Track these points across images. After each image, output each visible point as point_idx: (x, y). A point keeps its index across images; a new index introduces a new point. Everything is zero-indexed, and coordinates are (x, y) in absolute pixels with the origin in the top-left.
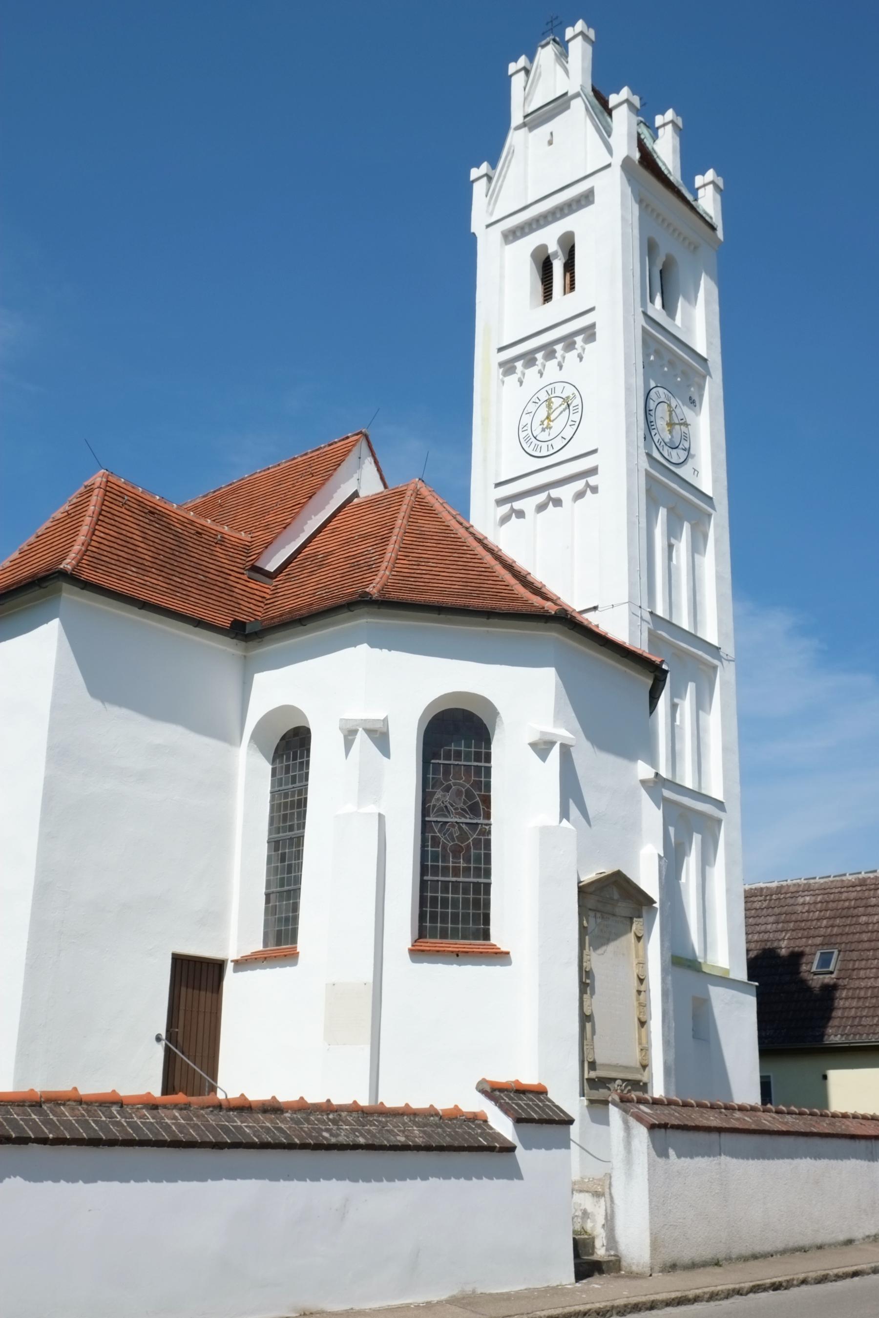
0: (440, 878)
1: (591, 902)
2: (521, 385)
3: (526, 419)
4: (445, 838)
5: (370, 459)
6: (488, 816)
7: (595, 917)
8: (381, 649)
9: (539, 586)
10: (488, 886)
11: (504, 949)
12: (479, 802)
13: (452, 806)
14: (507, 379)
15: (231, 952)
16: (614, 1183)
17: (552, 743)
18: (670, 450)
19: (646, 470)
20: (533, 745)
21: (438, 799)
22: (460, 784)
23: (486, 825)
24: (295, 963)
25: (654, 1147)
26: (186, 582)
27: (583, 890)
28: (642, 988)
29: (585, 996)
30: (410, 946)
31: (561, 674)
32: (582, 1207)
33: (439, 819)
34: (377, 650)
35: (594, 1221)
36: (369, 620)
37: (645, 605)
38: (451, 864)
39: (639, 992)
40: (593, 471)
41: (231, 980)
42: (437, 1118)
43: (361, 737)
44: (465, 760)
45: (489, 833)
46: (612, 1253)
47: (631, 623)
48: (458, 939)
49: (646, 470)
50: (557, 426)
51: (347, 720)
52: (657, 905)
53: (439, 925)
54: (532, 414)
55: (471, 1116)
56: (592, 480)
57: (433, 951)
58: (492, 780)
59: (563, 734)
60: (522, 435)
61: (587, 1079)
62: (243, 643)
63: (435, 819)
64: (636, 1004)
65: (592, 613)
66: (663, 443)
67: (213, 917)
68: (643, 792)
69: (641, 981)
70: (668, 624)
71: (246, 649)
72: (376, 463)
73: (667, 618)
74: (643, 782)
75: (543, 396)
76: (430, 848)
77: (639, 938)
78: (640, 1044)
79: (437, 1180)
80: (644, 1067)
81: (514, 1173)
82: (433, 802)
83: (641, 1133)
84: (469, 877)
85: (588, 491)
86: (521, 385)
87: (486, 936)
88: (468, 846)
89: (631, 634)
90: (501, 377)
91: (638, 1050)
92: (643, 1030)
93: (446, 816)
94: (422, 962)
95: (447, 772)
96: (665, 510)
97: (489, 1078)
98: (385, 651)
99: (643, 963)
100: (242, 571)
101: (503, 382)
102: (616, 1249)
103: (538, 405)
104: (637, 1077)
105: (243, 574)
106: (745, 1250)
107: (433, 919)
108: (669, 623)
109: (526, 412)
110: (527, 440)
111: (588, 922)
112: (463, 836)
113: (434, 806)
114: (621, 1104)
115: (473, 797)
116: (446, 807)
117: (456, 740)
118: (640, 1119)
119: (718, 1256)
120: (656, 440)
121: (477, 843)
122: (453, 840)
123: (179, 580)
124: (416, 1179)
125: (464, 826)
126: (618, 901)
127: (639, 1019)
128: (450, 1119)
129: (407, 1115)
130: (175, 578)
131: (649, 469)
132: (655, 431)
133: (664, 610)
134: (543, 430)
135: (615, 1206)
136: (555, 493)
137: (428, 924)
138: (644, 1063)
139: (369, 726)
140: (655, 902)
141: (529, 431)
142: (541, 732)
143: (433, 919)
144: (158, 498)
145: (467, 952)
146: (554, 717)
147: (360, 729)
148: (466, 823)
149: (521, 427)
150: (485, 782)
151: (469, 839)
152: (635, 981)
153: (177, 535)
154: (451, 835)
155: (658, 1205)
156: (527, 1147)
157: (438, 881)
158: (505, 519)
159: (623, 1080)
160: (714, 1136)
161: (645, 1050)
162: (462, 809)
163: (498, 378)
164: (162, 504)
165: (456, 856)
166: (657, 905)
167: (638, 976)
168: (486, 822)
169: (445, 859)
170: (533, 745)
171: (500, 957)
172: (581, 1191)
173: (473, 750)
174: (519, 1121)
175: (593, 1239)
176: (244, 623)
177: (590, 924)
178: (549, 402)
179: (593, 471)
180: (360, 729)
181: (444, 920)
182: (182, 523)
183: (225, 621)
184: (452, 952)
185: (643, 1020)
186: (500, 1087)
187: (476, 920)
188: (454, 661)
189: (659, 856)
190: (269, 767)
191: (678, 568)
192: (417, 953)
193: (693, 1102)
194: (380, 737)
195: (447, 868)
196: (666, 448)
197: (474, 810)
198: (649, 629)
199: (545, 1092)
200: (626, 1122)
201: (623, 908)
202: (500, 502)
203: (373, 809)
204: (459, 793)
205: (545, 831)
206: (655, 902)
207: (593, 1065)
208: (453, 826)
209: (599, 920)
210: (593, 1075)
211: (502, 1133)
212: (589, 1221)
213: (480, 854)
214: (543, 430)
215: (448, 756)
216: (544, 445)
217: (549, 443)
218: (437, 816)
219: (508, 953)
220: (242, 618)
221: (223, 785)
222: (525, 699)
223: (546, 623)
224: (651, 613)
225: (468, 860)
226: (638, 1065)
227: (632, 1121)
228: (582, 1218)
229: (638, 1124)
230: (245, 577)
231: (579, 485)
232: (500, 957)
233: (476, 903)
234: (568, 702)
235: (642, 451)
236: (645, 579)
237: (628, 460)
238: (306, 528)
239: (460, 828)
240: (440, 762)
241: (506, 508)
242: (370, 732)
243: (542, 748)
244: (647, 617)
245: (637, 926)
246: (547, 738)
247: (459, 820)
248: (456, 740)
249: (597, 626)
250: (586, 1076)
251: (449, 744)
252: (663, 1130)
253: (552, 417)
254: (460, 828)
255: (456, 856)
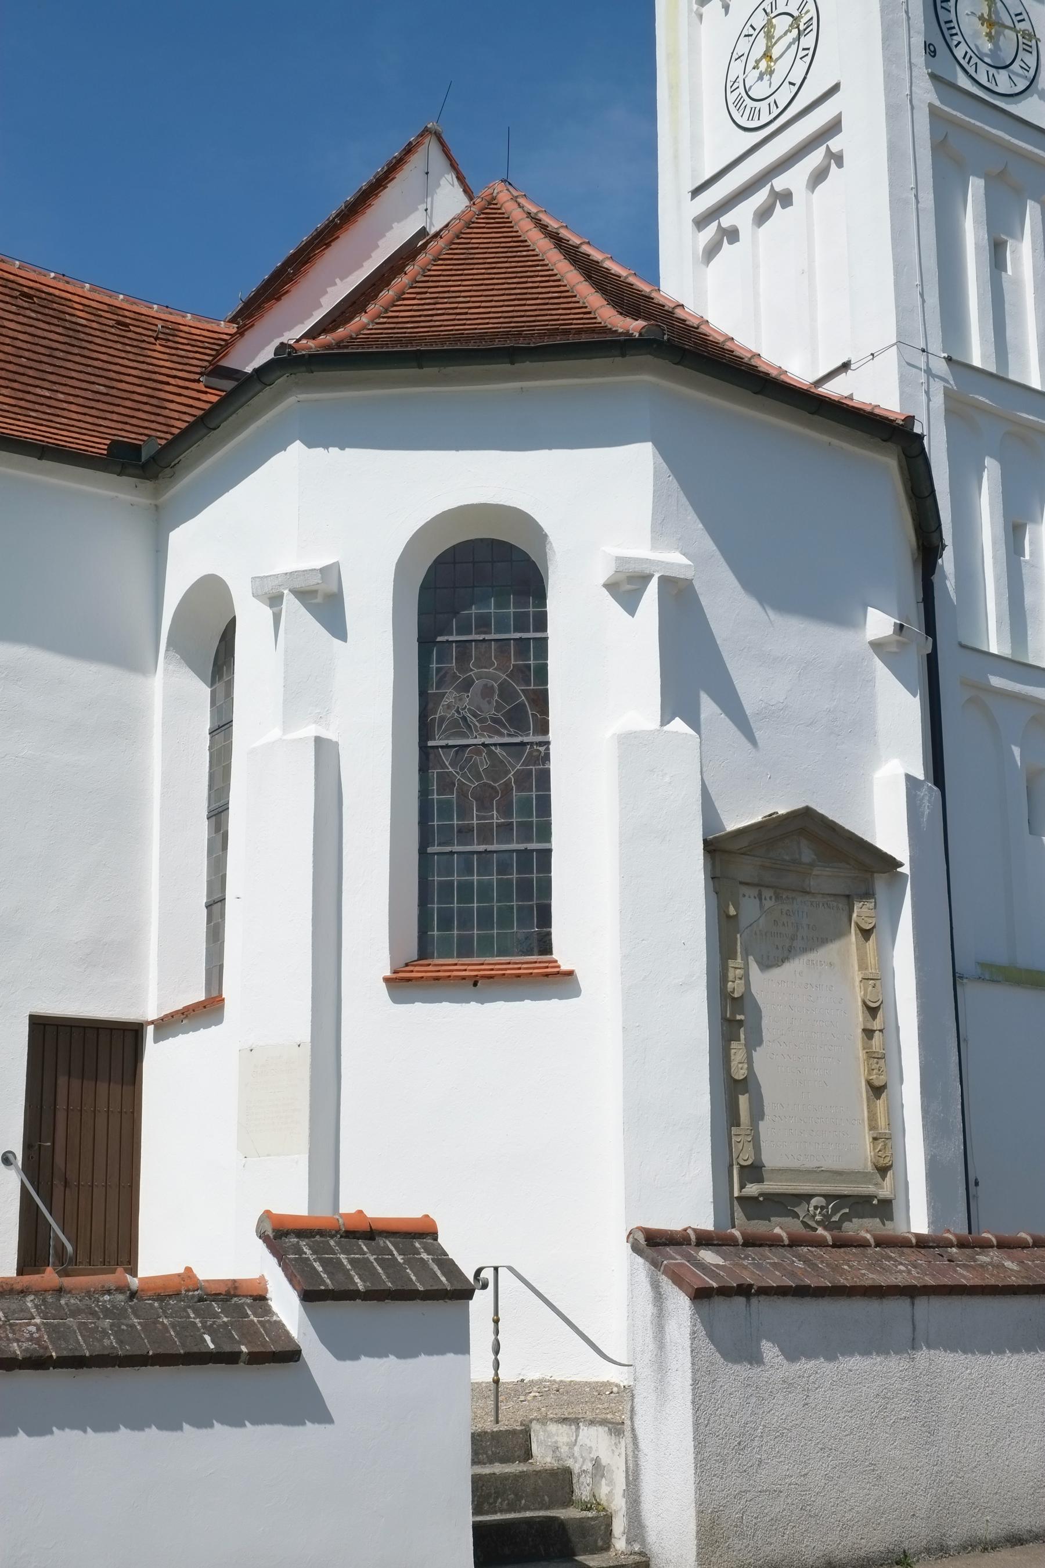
0: (457, 848)
1: (746, 868)
2: (727, 13)
3: (737, 67)
4: (464, 776)
5: (451, 177)
6: (543, 727)
7: (760, 897)
8: (326, 447)
9: (694, 322)
10: (546, 856)
11: (565, 967)
12: (527, 704)
13: (475, 715)
14: (704, 10)
15: (149, 1009)
16: (638, 1408)
17: (646, 578)
18: (992, 71)
19: (931, 105)
20: (611, 587)
21: (449, 707)
22: (488, 676)
23: (540, 744)
24: (219, 1020)
25: (711, 1336)
26: (61, 396)
27: (720, 851)
28: (877, 1025)
29: (734, 1045)
30: (388, 973)
31: (664, 450)
32: (593, 1455)
33: (451, 742)
34: (320, 451)
35: (611, 1483)
36: (302, 397)
37: (936, 346)
38: (475, 822)
39: (869, 1033)
40: (834, 127)
41: (159, 1059)
42: (120, 1297)
43: (290, 604)
44: (498, 631)
45: (547, 757)
46: (637, 1548)
47: (903, 380)
48: (493, 956)
49: (931, 105)
50: (781, 68)
51: (261, 578)
52: (905, 869)
53: (455, 932)
54: (744, 58)
55: (223, 1290)
56: (835, 144)
57: (428, 978)
58: (549, 662)
59: (674, 559)
60: (731, 98)
61: (739, 1198)
62: (149, 484)
63: (443, 743)
64: (862, 1054)
65: (842, 377)
66: (975, 60)
67: (115, 950)
68: (878, 664)
69: (872, 1011)
70: (998, 380)
71: (156, 494)
72: (461, 178)
73: (993, 369)
74: (877, 646)
75: (759, 20)
76: (435, 796)
77: (866, 934)
78: (873, 1127)
79: (77, 1434)
80: (883, 1170)
81: (311, 1408)
82: (440, 712)
83: (680, 1304)
84: (510, 841)
85: (833, 166)
86: (727, 13)
87: (545, 947)
88: (507, 784)
89: (904, 397)
90: (695, 7)
91: (868, 1140)
92: (880, 1104)
93: (464, 735)
94: (439, 1001)
95: (463, 657)
96: (1038, 207)
97: (275, 1211)
98: (334, 451)
99: (878, 979)
100: (197, 377)
101: (701, 16)
102: (643, 1542)
103: (752, 39)
104: (868, 1189)
105: (198, 381)
106: (991, 1527)
107: (446, 923)
108: (1000, 379)
109: (735, 56)
110: (739, 103)
111: (736, 908)
112: (498, 769)
113: (442, 719)
114: (649, 1251)
115: (515, 695)
116: (464, 718)
117: (477, 600)
118: (678, 1280)
119: (906, 1545)
120: (959, 53)
121: (523, 779)
122: (478, 777)
123: (47, 394)
124: (15, 1433)
125: (498, 750)
126: (812, 865)
127: (869, 1083)
128: (160, 1298)
129: (36, 1293)
130: (38, 391)
131: (937, 103)
132: (958, 38)
133: (984, 357)
134: (761, 78)
135: (641, 1455)
136: (779, 183)
137: (436, 933)
138: (882, 1162)
139: (300, 584)
140: (901, 865)
141: (742, 90)
142: (618, 558)
143: (446, 923)
144: (52, 275)
145: (491, 977)
146: (653, 531)
147: (286, 592)
148: (501, 745)
149: (729, 84)
150: (536, 666)
151: (508, 772)
152: (859, 1016)
153: (74, 329)
154: (474, 769)
155: (716, 1449)
156: (344, 1348)
157: (452, 853)
158: (712, 251)
159: (824, 1196)
160: (899, 1306)
161: (886, 1139)
162: (495, 720)
163: (690, 10)
164: (61, 285)
165: (484, 806)
166: (905, 869)
167: (864, 1003)
168: (540, 738)
169: (464, 813)
170: (611, 587)
171: (561, 982)
172: (592, 1423)
173: (512, 610)
174: (309, 1296)
175: (608, 1521)
176: (138, 448)
177: (750, 908)
178: (769, 26)
179: (834, 127)
180: (286, 592)
181: (465, 923)
182: (94, 312)
183: (101, 448)
184: (464, 978)
185: (877, 1083)
186: (299, 1226)
187: (524, 915)
188: (461, 453)
189: (909, 778)
190: (207, 691)
191: (1018, 282)
192: (402, 984)
193: (868, 1236)
194: (324, 601)
195: (469, 829)
196: (983, 68)
197: (516, 719)
198: (948, 394)
199: (434, 1235)
200: (656, 1286)
201: (827, 879)
202: (701, 222)
203: (311, 731)
204: (487, 692)
205: (629, 743)
206: (901, 865)
207: (754, 1172)
208: (479, 753)
209: (768, 904)
210: (752, 1189)
211: (285, 1322)
212: (604, 1481)
213: (529, 800)
214: (761, 78)
215: (464, 629)
216: (763, 105)
217: (771, 100)
218: (447, 738)
219: (570, 973)
220: (129, 437)
221: (125, 727)
222: (597, 504)
223: (623, 355)
224: (949, 360)
225: (506, 810)
226: (870, 1168)
227: (667, 1286)
228: (593, 1476)
229: (676, 1289)
230: (201, 386)
231: (815, 158)
232: (561, 982)
233: (525, 889)
234: (684, 500)
235: (922, 71)
236: (933, 300)
237: (889, 90)
238: (323, 300)
239: (491, 754)
240: (451, 638)
241: (712, 229)
242: (304, 595)
243: (626, 588)
244: (940, 367)
245: (861, 911)
246: (633, 568)
247: (488, 741)
248: (477, 600)
249: (850, 397)
250: (736, 1194)
251: (470, 608)
252: (742, 1300)
253: (776, 52)
254: (491, 754)
255: (484, 806)
